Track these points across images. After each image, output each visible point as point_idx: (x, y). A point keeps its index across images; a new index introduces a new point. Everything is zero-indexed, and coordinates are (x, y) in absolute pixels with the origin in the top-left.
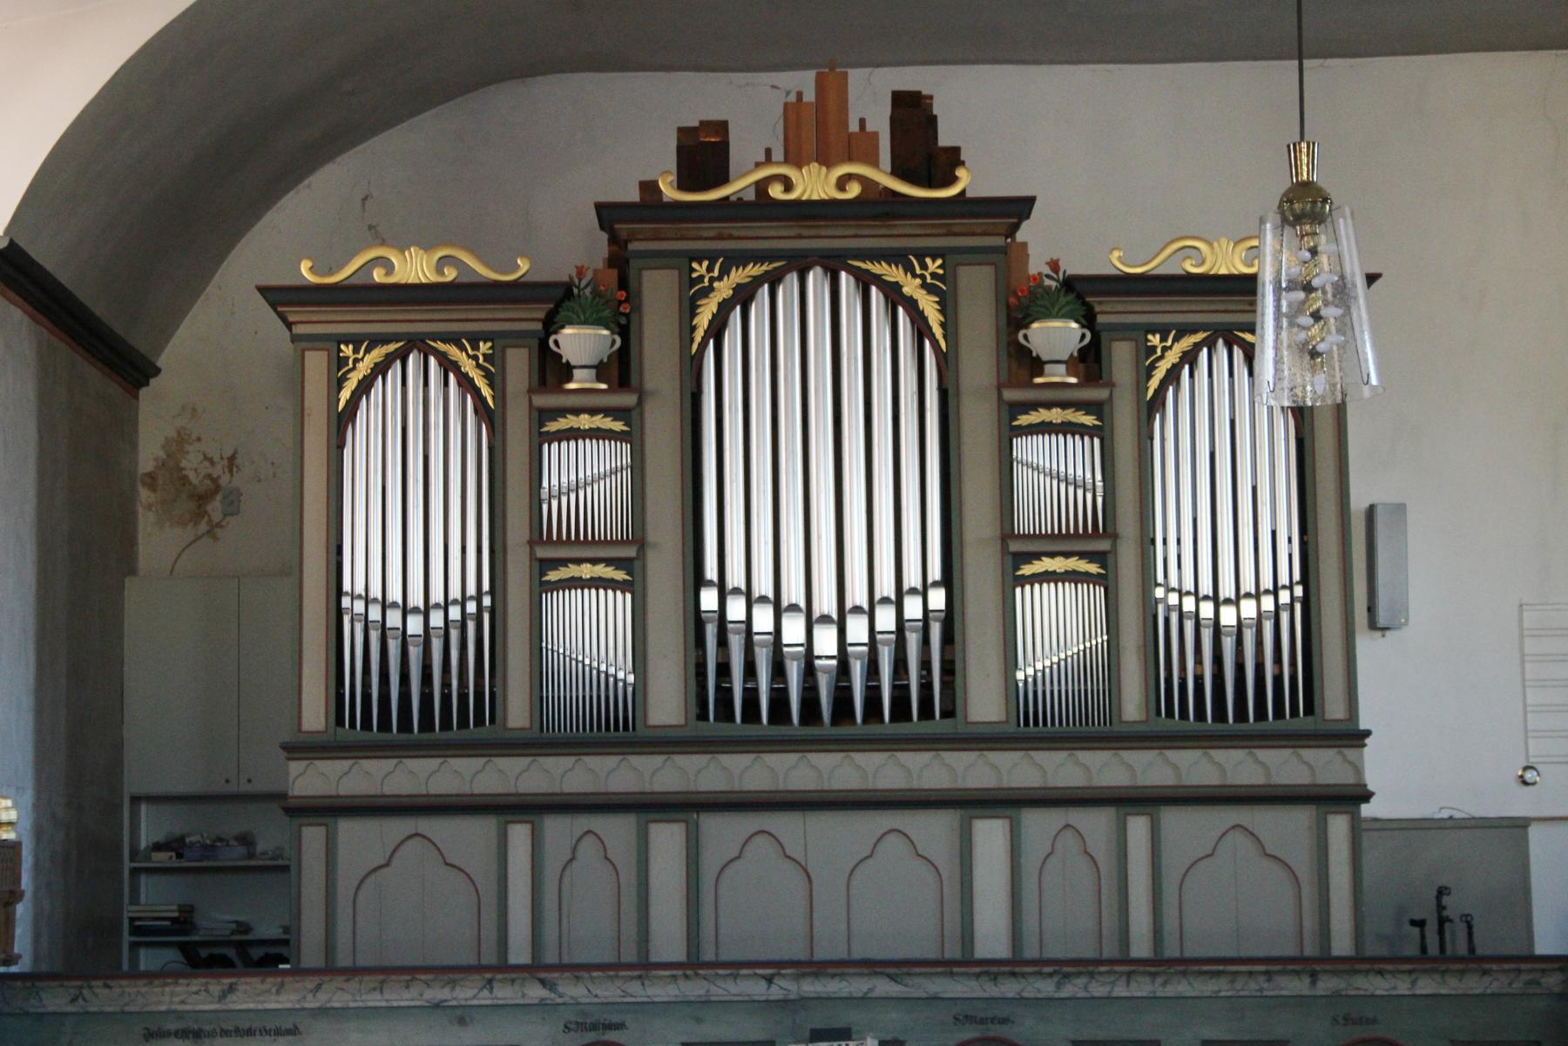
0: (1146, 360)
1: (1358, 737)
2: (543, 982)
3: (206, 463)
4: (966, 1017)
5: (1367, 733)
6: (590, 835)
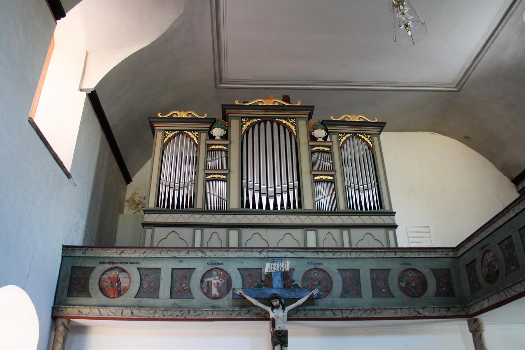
0: (339, 139)
1: (393, 214)
2: (202, 252)
3: (140, 198)
4: (311, 263)
5: (395, 213)
6: (215, 233)
